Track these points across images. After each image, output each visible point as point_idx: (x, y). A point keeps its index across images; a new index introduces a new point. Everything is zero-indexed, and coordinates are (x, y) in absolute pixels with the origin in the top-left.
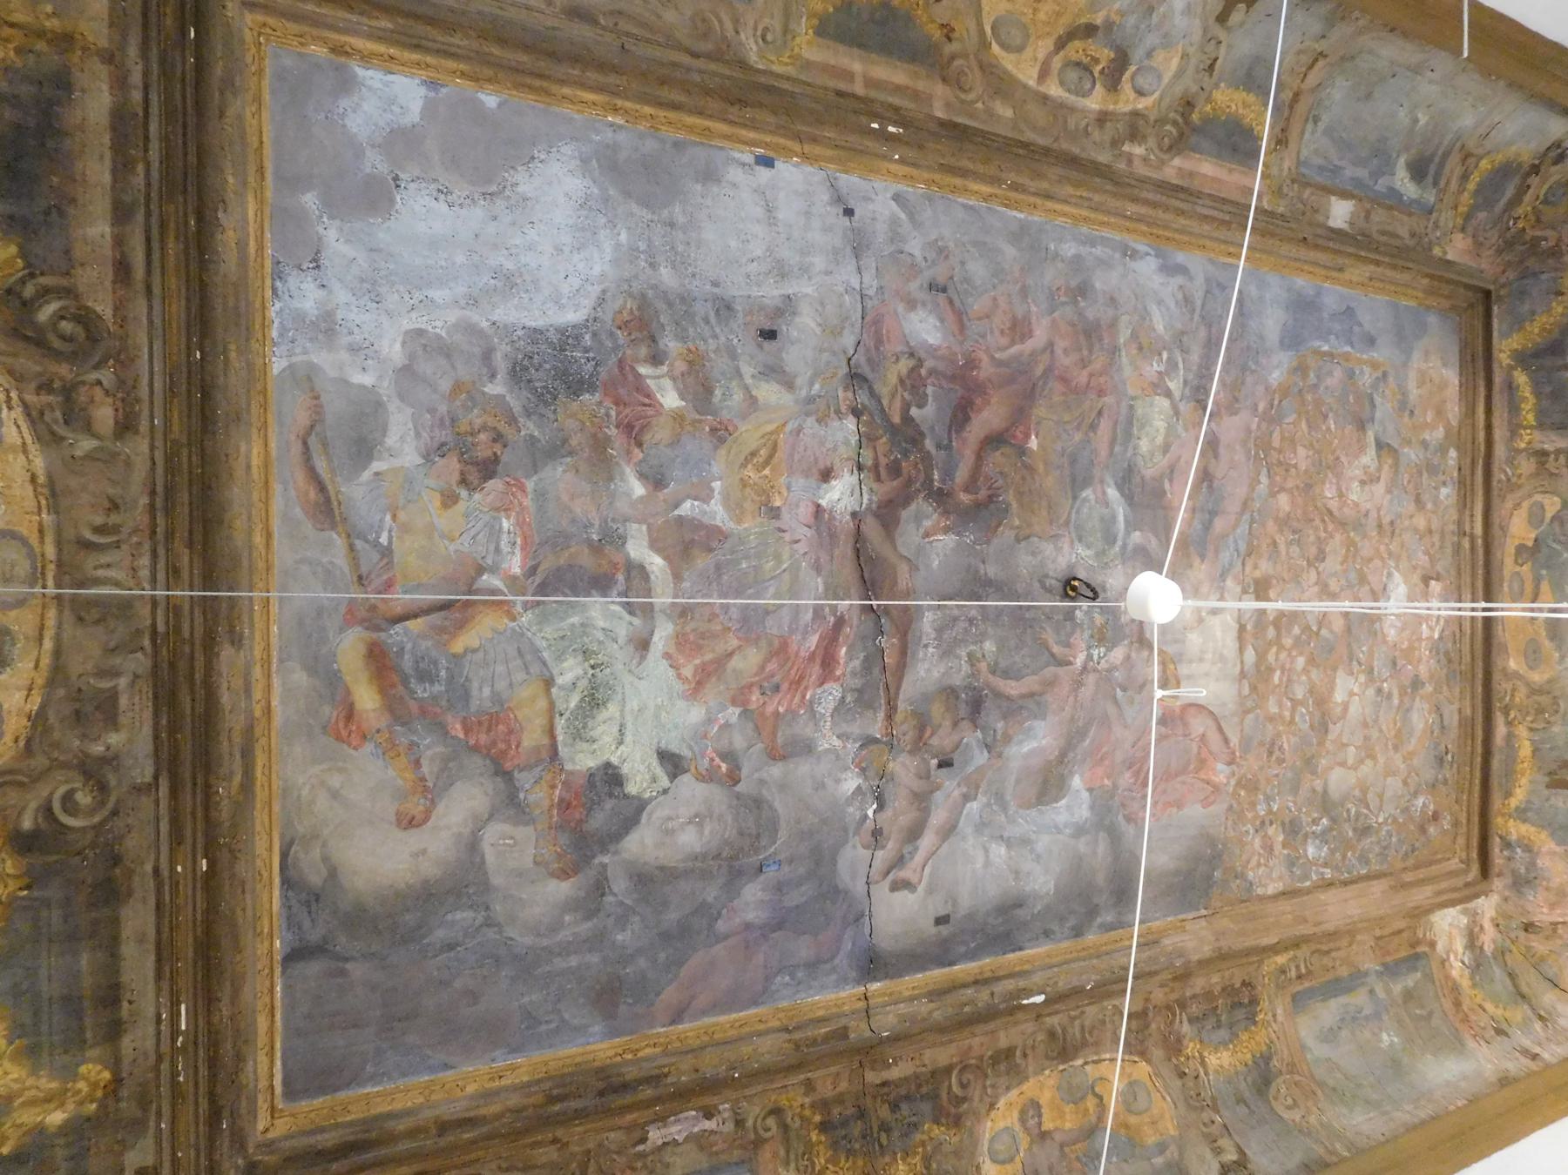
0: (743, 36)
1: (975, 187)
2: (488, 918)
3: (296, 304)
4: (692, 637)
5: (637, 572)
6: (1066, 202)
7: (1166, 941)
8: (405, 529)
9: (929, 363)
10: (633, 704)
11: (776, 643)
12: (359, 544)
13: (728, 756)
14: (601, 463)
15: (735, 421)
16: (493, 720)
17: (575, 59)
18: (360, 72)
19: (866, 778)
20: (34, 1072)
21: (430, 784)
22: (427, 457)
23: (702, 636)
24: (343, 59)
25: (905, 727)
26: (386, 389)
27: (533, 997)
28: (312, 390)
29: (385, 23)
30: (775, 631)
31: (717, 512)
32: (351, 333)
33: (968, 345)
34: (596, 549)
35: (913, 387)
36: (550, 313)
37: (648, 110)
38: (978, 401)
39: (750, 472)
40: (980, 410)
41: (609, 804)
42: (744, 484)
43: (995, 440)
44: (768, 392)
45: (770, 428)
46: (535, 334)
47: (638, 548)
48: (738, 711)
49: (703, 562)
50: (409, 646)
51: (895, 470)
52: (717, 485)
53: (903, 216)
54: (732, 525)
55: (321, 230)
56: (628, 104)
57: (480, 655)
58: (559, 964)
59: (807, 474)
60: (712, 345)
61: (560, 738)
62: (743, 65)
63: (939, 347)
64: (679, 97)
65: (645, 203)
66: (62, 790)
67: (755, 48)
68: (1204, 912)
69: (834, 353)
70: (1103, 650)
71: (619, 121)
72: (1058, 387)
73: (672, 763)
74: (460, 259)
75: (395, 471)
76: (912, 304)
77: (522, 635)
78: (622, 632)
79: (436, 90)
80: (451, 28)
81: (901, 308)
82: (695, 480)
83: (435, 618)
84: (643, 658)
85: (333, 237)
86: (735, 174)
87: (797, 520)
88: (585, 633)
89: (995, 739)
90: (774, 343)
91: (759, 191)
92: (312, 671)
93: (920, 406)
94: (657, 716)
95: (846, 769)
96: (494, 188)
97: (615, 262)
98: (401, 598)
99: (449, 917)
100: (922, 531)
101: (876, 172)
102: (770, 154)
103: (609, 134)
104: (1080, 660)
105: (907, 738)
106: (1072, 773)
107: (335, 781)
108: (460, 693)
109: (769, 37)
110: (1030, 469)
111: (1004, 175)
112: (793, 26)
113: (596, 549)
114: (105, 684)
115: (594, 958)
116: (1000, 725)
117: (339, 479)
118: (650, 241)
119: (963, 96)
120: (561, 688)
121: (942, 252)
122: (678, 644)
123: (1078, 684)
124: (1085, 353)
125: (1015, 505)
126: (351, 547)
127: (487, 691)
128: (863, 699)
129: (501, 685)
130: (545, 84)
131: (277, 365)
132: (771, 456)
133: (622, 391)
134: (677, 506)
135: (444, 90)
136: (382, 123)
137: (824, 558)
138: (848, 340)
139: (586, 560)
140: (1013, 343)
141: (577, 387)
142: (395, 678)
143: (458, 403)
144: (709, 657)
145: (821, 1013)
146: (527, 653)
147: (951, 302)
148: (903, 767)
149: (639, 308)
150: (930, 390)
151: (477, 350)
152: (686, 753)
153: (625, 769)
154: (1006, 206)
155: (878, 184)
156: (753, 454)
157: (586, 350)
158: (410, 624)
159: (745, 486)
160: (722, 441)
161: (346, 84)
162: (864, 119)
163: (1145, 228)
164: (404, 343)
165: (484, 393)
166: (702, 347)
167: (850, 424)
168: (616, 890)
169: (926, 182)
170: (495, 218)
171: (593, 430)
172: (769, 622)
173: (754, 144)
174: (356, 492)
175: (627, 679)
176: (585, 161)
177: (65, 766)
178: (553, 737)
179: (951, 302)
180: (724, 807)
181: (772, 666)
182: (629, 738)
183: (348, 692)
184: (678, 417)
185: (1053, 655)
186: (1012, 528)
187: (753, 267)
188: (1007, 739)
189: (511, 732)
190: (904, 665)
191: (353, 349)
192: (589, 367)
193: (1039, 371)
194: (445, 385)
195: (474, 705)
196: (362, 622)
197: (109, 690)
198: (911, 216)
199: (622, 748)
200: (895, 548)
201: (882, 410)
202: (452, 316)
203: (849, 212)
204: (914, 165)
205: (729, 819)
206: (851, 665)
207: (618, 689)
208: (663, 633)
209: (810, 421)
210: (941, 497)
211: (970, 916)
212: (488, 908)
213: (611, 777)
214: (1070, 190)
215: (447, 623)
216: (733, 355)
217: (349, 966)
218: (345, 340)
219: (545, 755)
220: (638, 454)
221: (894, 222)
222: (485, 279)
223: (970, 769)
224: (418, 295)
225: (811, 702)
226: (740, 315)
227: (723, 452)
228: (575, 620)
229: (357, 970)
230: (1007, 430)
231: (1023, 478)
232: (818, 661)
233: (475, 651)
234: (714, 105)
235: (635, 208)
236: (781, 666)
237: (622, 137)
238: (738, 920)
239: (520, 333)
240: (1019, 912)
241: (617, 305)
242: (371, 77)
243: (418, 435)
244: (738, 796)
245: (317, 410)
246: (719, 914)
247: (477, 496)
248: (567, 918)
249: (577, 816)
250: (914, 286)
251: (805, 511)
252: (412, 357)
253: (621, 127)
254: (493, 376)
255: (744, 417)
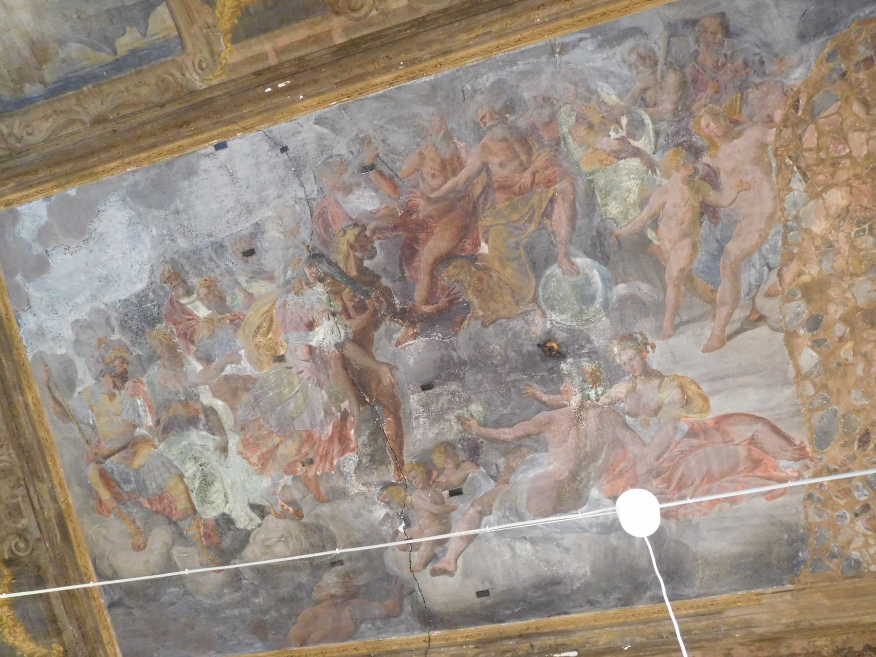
0: (188, 75)
1: (378, 80)
2: (185, 591)
3: (27, 327)
4: (251, 441)
5: (210, 411)
6: (467, 47)
7: (730, 613)
8: (98, 415)
9: (371, 226)
10: (228, 482)
11: (304, 435)
12: (82, 426)
13: (291, 503)
14: (176, 359)
15: (243, 311)
16: (161, 499)
17: (92, 153)
18: (19, 208)
19: (391, 508)
20: (38, 645)
21: (142, 530)
22: (97, 379)
23: (258, 438)
24: (11, 207)
25: (413, 473)
26: (72, 353)
27: (220, 629)
28: (44, 363)
29: (12, 185)
30: (301, 428)
31: (246, 367)
32: (50, 332)
33: (403, 199)
34: (185, 404)
35: (361, 247)
36: (129, 289)
37: (143, 155)
38: (422, 236)
39: (260, 339)
40: (425, 242)
41: (230, 534)
42: (258, 347)
43: (444, 260)
44: (260, 288)
45: (265, 309)
46: (126, 302)
47: (207, 399)
48: (291, 477)
49: (246, 397)
50: (115, 469)
51: (361, 308)
52: (242, 352)
53: (325, 131)
54: (257, 372)
55: (26, 290)
56: (132, 158)
57: (146, 468)
58: (228, 613)
59: (297, 329)
60: (218, 272)
61: (195, 503)
62: (193, 92)
63: (378, 211)
64: (153, 140)
65: (160, 207)
66: (14, 542)
67: (197, 78)
68: (790, 587)
69: (296, 247)
70: (600, 390)
71: (134, 168)
72: (500, 199)
73: (260, 510)
74: (83, 278)
75: (86, 389)
76: (348, 189)
77: (162, 455)
78: (211, 445)
79: (50, 200)
80: (36, 171)
81: (339, 196)
82: (228, 353)
83: (122, 453)
84: (226, 457)
85: (32, 291)
86: (205, 163)
87: (297, 358)
88: (192, 449)
89: (498, 472)
90: (254, 256)
91: (223, 167)
92: (80, 485)
93: (371, 258)
94: (243, 486)
95: (374, 504)
96: (87, 236)
97: (153, 247)
98: (106, 447)
99: (168, 590)
100: (394, 342)
101: (298, 111)
102: (221, 140)
103: (131, 178)
104: (575, 401)
105: (417, 479)
106: (587, 487)
107: (104, 531)
108: (142, 488)
109: (204, 66)
110: (486, 269)
111: (394, 61)
112: (216, 49)
113: (185, 404)
114: (14, 501)
115: (247, 611)
116: (501, 461)
117: (65, 399)
118: (169, 229)
119: (356, 15)
120: (188, 478)
121: (366, 141)
122: (244, 446)
123: (577, 419)
124: (523, 157)
125: (476, 301)
126: (80, 429)
127: (154, 485)
128: (376, 459)
129: (159, 480)
130: (90, 171)
131: (30, 356)
132: (271, 325)
133: (176, 317)
134: (222, 370)
135: (53, 198)
136: (34, 229)
137: (323, 378)
138: (305, 234)
139: (181, 411)
140: (446, 180)
141: (152, 321)
142: (114, 484)
143: (102, 349)
144: (265, 450)
145: (395, 648)
146: (167, 465)
147: (381, 173)
148: (420, 499)
149: (173, 268)
150: (376, 244)
151: (103, 321)
152: (266, 504)
153: (234, 516)
154: (413, 78)
155: (301, 119)
156: (259, 328)
157: (152, 301)
158: (113, 458)
159: (259, 348)
160: (238, 326)
161: (15, 217)
162: (259, 90)
163: (570, 20)
164: (72, 329)
165: (111, 341)
166: (212, 275)
167: (320, 288)
168: (247, 577)
169: (337, 99)
170: (91, 251)
171: (167, 342)
172: (296, 423)
173: (211, 139)
174: (74, 403)
175: (221, 468)
176: (123, 200)
177: (11, 534)
178: (192, 503)
179: (381, 173)
180: (297, 532)
181: (305, 449)
182: (231, 499)
183: (97, 493)
184: (209, 320)
185: (544, 403)
186: (477, 318)
187: (230, 216)
188: (511, 470)
189: (171, 503)
190: (402, 434)
191: (54, 339)
192: (156, 309)
193: (478, 189)
194: (95, 343)
195: (151, 492)
196: (93, 461)
197: (15, 503)
198: (333, 129)
199: (228, 505)
200: (373, 358)
201: (341, 272)
202: (88, 308)
203: (284, 149)
204: (320, 94)
205: (303, 538)
206: (361, 440)
207: (217, 474)
208: (234, 441)
209: (291, 296)
210: (405, 315)
211: (510, 591)
212: (184, 586)
213: (226, 521)
214: (464, 37)
215: (128, 455)
216: (230, 273)
217: (132, 611)
218: (49, 336)
219: (190, 512)
220: (193, 348)
221: (320, 138)
222: (97, 284)
223: (480, 494)
224: (71, 304)
225: (338, 466)
226: (229, 248)
227: (240, 332)
228: (185, 443)
229: (137, 613)
230: (455, 247)
231: (480, 280)
232: (336, 440)
233: (143, 466)
234: (170, 134)
235: (155, 212)
236: (312, 447)
237: (138, 176)
238: (324, 593)
239: (119, 304)
240: (558, 588)
241: (160, 271)
242: (23, 209)
243: (90, 370)
244: (305, 525)
245: (48, 371)
246: (312, 590)
247: (123, 392)
248: (226, 591)
249: (216, 541)
250: (346, 177)
251: (302, 352)
252: (77, 334)
253: (136, 171)
254: (113, 331)
255: (248, 307)
